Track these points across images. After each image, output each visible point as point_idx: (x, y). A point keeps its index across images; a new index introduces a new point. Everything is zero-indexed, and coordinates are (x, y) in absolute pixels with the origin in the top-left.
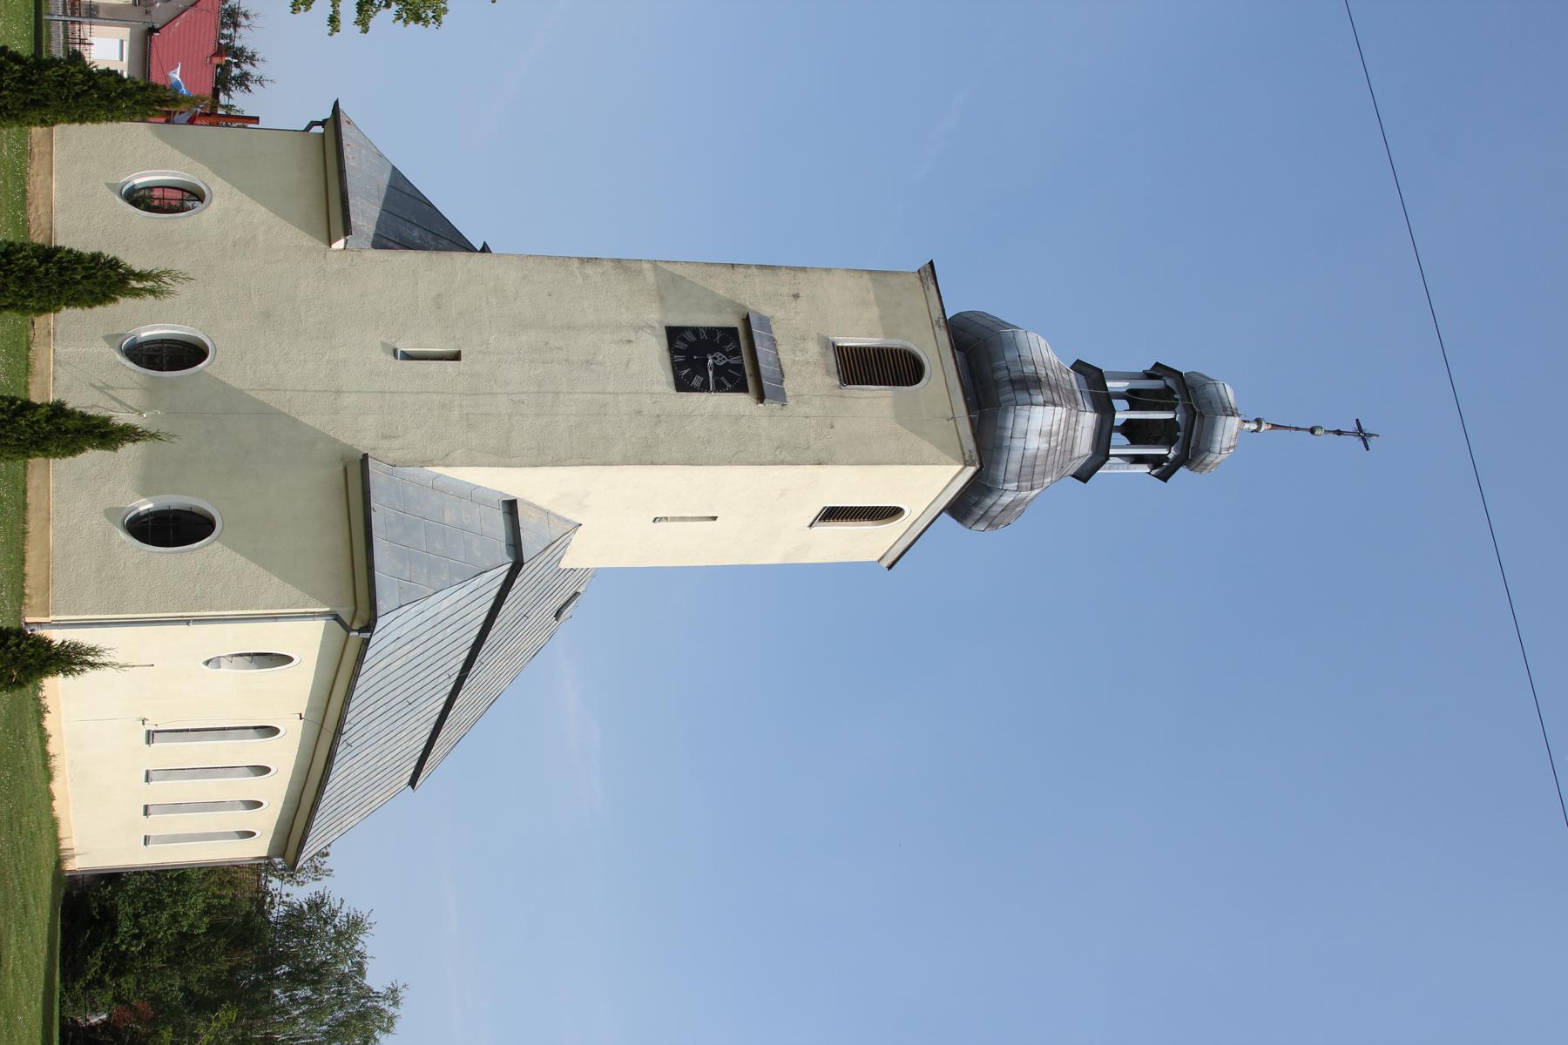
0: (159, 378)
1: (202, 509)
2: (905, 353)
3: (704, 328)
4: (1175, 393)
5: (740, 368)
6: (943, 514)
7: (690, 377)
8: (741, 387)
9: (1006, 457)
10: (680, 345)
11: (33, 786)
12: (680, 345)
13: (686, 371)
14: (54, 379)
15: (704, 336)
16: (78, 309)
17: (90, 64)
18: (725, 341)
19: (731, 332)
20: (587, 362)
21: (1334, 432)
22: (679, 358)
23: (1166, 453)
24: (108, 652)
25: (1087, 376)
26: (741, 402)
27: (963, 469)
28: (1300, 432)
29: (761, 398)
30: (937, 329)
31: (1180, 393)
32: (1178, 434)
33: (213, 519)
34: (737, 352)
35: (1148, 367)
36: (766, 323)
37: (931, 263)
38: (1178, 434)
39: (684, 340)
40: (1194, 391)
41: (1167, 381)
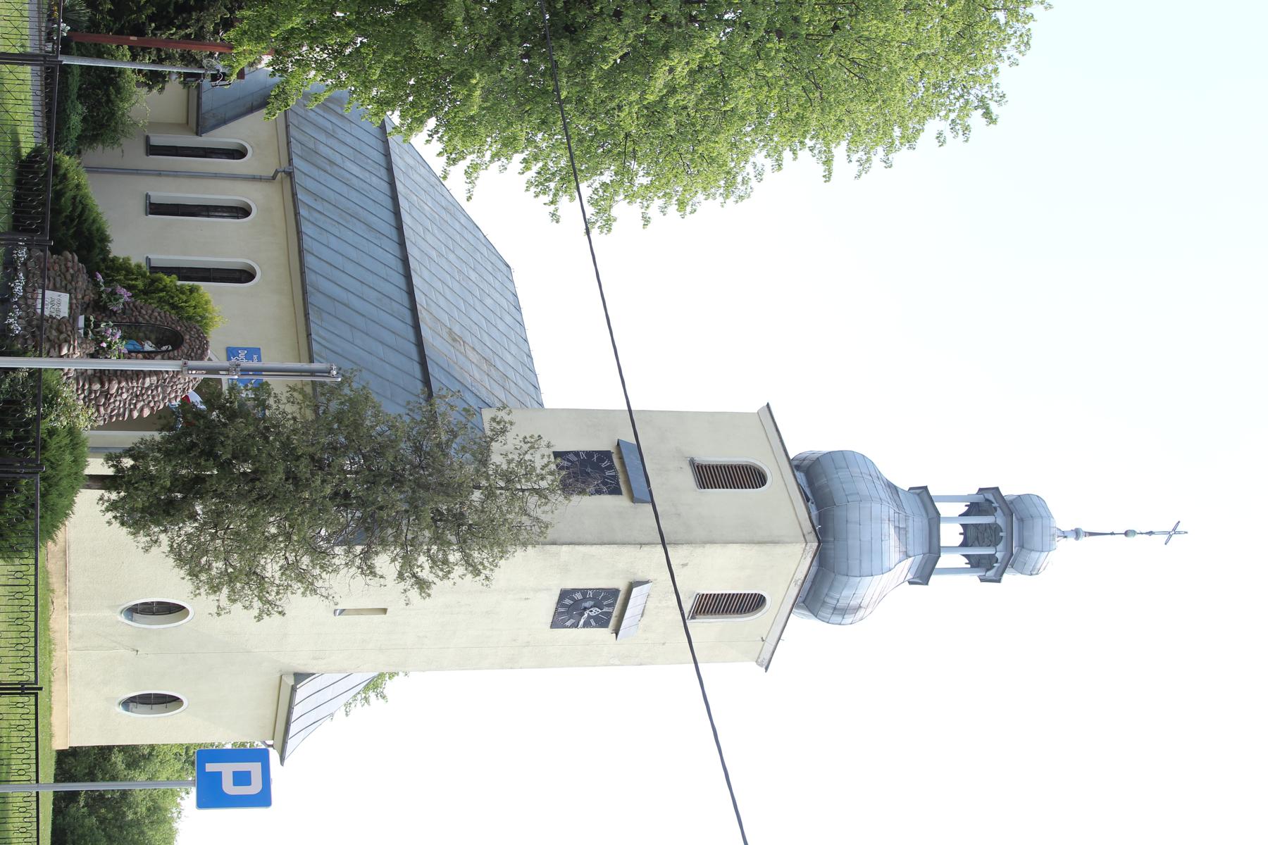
0: (150, 629)
3: (583, 452)
4: (1002, 532)
5: (615, 478)
8: (616, 491)
11: (200, 342)
14: (70, 632)
18: (601, 460)
19: (606, 455)
20: (487, 612)
21: (1147, 533)
23: (994, 553)
26: (619, 502)
28: (1116, 536)
29: (633, 499)
30: (793, 584)
32: (1001, 534)
34: (611, 467)
37: (768, 405)
38: (1001, 534)
40: (1021, 520)
41: (997, 519)
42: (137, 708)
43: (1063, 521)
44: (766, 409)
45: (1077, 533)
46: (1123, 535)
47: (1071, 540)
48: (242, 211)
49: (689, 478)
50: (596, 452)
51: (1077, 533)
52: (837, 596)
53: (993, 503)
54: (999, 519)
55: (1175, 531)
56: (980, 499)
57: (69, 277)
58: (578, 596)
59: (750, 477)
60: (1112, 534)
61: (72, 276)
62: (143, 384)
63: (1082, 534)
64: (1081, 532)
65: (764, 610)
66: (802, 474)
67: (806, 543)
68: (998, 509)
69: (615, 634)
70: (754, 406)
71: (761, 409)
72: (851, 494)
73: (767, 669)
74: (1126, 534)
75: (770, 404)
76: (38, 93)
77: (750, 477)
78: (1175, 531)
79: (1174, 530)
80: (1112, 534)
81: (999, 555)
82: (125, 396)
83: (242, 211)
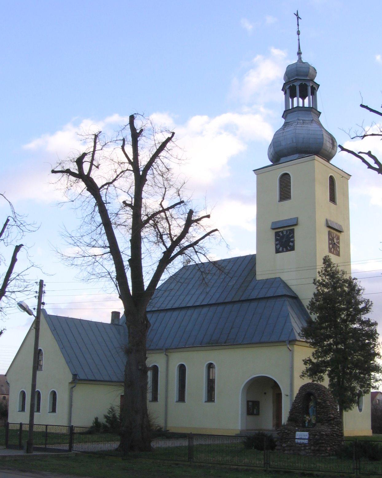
1: (206, 368)
2: (281, 180)
5: (287, 231)
6: (330, 162)
7: (290, 246)
8: (292, 231)
9: (297, 322)
10: (281, 249)
12: (281, 249)
13: (289, 248)
15: (277, 242)
16: (290, 411)
17: (158, 442)
19: (277, 234)
22: (285, 249)
24: (72, 253)
25: (286, 125)
27: (316, 160)
29: (296, 225)
31: (291, 84)
32: (303, 83)
33: (180, 365)
34: (282, 232)
35: (283, 93)
36: (273, 223)
37: (254, 171)
38: (303, 83)
39: (279, 248)
42: (21, 424)
43: (295, 60)
44: (255, 171)
45: (299, 53)
46: (299, 35)
47: (302, 56)
48: (182, 369)
49: (286, 203)
50: (275, 237)
51: (299, 53)
52: (329, 148)
53: (290, 86)
54: (297, 84)
55: (297, 15)
56: (288, 92)
57: (289, 432)
58: (331, 246)
59: (285, 180)
60: (299, 40)
61: (288, 431)
62: (329, 406)
63: (300, 52)
64: (299, 52)
65: (334, 176)
66: (282, 159)
67: (314, 159)
68: (293, 84)
69: (342, 233)
70: (254, 177)
71: (255, 174)
72: (292, 140)
73: (351, 176)
74: (298, 34)
75: (253, 170)
76: (101, 449)
77: (285, 180)
78: (297, 15)
79: (299, 17)
80: (299, 40)
81: (311, 85)
82: (333, 412)
83: (182, 369)
